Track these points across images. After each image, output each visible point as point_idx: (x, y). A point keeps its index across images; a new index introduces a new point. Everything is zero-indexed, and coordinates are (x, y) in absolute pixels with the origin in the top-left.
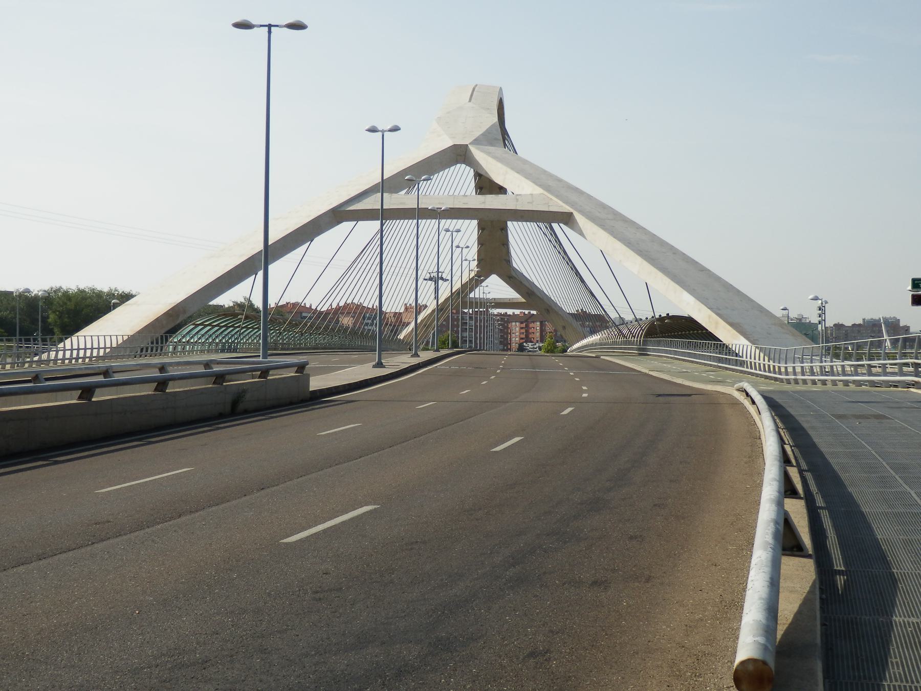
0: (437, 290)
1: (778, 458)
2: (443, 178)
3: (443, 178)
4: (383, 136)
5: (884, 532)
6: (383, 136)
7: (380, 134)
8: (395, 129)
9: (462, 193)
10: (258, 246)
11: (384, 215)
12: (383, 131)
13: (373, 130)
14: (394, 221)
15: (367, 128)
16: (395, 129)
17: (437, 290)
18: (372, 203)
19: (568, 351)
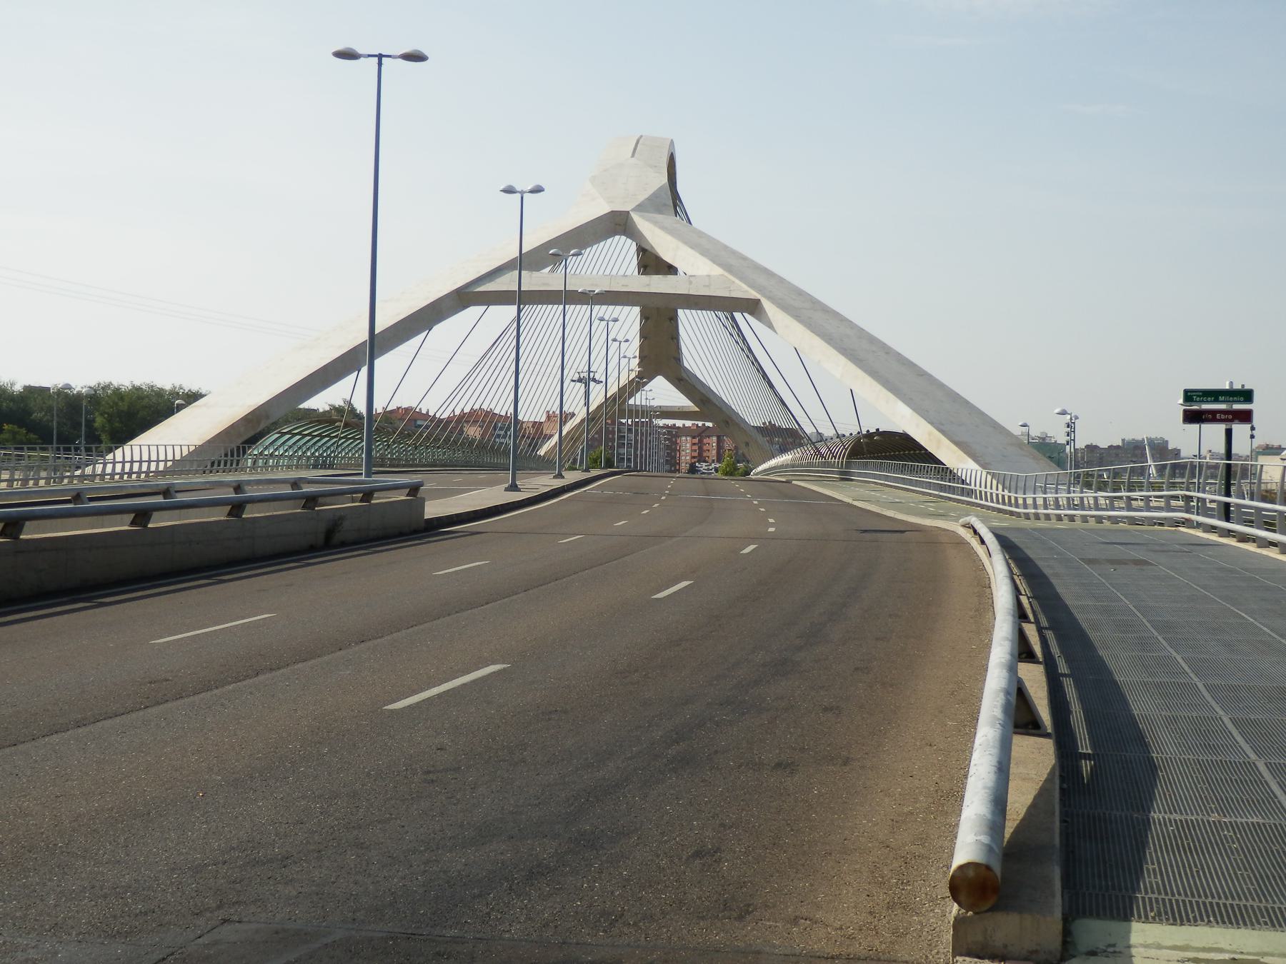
0: (587, 394)
4: (522, 198)
6: (522, 198)
7: (518, 196)
8: (537, 190)
11: (522, 298)
12: (522, 193)
13: (509, 190)
14: (531, 306)
16: (537, 190)
17: (587, 394)
18: (507, 283)
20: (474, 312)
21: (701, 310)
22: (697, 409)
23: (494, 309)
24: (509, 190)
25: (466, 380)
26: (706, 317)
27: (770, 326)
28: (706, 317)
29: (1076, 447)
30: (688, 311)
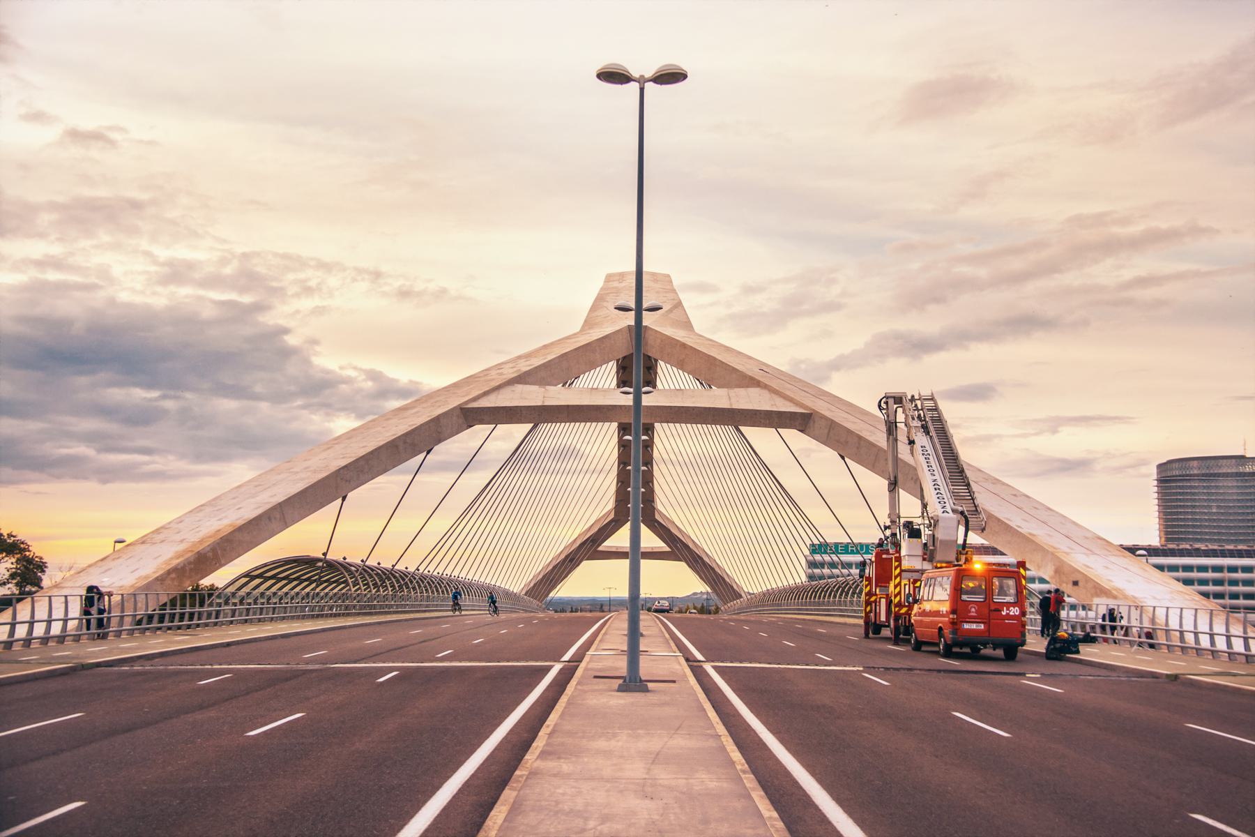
0: (633, 653)
1: (69, 307)
2: (543, 429)
3: (543, 429)
4: (642, 90)
5: (1086, 573)
6: (642, 90)
7: (634, 87)
8: (671, 77)
9: (590, 387)
10: (545, 428)
11: (540, 415)
12: (642, 81)
13: (613, 76)
14: (546, 424)
15: (599, 65)
16: (671, 77)
17: (633, 653)
18: (532, 396)
19: (893, 598)
20: (481, 430)
21: (668, 422)
22: (668, 549)
23: (502, 428)
24: (613, 76)
25: (463, 516)
26: (680, 432)
27: (902, 454)
28: (680, 432)
29: (1157, 631)
30: (679, 424)
